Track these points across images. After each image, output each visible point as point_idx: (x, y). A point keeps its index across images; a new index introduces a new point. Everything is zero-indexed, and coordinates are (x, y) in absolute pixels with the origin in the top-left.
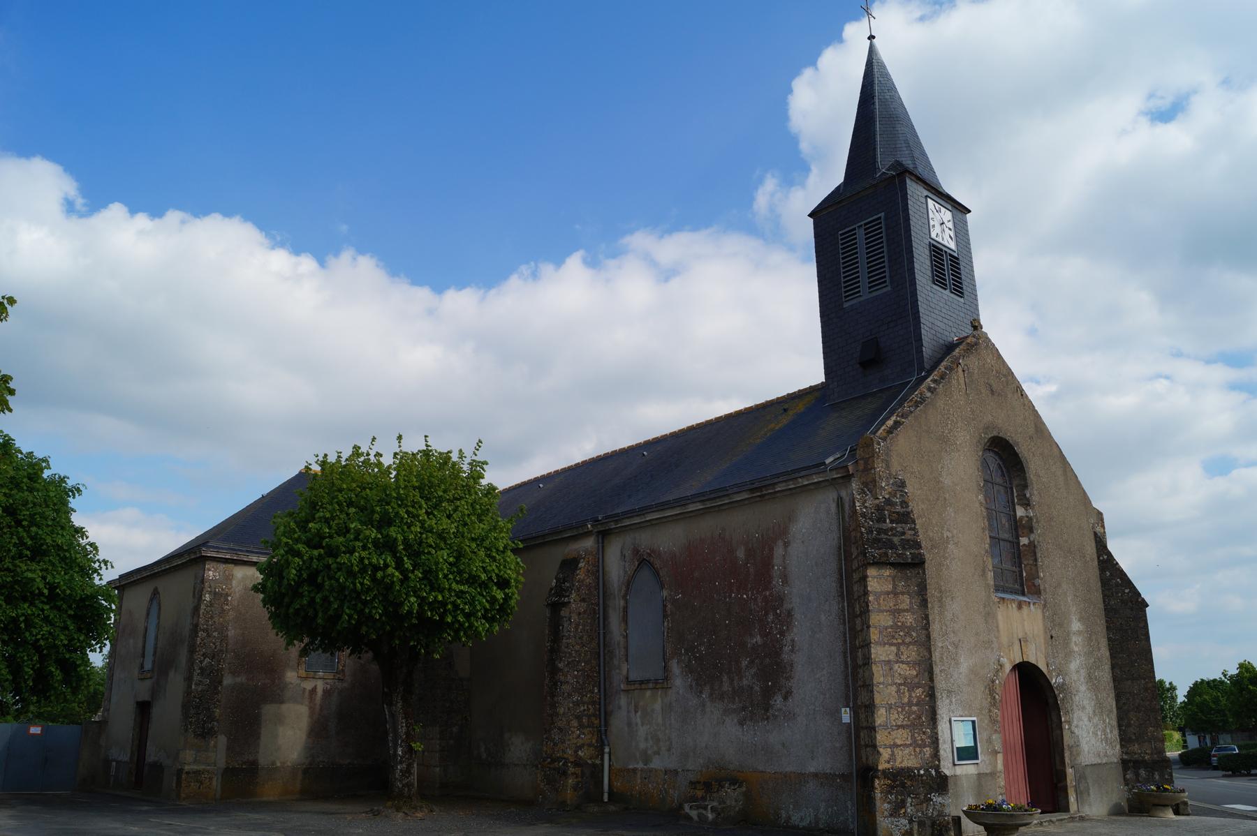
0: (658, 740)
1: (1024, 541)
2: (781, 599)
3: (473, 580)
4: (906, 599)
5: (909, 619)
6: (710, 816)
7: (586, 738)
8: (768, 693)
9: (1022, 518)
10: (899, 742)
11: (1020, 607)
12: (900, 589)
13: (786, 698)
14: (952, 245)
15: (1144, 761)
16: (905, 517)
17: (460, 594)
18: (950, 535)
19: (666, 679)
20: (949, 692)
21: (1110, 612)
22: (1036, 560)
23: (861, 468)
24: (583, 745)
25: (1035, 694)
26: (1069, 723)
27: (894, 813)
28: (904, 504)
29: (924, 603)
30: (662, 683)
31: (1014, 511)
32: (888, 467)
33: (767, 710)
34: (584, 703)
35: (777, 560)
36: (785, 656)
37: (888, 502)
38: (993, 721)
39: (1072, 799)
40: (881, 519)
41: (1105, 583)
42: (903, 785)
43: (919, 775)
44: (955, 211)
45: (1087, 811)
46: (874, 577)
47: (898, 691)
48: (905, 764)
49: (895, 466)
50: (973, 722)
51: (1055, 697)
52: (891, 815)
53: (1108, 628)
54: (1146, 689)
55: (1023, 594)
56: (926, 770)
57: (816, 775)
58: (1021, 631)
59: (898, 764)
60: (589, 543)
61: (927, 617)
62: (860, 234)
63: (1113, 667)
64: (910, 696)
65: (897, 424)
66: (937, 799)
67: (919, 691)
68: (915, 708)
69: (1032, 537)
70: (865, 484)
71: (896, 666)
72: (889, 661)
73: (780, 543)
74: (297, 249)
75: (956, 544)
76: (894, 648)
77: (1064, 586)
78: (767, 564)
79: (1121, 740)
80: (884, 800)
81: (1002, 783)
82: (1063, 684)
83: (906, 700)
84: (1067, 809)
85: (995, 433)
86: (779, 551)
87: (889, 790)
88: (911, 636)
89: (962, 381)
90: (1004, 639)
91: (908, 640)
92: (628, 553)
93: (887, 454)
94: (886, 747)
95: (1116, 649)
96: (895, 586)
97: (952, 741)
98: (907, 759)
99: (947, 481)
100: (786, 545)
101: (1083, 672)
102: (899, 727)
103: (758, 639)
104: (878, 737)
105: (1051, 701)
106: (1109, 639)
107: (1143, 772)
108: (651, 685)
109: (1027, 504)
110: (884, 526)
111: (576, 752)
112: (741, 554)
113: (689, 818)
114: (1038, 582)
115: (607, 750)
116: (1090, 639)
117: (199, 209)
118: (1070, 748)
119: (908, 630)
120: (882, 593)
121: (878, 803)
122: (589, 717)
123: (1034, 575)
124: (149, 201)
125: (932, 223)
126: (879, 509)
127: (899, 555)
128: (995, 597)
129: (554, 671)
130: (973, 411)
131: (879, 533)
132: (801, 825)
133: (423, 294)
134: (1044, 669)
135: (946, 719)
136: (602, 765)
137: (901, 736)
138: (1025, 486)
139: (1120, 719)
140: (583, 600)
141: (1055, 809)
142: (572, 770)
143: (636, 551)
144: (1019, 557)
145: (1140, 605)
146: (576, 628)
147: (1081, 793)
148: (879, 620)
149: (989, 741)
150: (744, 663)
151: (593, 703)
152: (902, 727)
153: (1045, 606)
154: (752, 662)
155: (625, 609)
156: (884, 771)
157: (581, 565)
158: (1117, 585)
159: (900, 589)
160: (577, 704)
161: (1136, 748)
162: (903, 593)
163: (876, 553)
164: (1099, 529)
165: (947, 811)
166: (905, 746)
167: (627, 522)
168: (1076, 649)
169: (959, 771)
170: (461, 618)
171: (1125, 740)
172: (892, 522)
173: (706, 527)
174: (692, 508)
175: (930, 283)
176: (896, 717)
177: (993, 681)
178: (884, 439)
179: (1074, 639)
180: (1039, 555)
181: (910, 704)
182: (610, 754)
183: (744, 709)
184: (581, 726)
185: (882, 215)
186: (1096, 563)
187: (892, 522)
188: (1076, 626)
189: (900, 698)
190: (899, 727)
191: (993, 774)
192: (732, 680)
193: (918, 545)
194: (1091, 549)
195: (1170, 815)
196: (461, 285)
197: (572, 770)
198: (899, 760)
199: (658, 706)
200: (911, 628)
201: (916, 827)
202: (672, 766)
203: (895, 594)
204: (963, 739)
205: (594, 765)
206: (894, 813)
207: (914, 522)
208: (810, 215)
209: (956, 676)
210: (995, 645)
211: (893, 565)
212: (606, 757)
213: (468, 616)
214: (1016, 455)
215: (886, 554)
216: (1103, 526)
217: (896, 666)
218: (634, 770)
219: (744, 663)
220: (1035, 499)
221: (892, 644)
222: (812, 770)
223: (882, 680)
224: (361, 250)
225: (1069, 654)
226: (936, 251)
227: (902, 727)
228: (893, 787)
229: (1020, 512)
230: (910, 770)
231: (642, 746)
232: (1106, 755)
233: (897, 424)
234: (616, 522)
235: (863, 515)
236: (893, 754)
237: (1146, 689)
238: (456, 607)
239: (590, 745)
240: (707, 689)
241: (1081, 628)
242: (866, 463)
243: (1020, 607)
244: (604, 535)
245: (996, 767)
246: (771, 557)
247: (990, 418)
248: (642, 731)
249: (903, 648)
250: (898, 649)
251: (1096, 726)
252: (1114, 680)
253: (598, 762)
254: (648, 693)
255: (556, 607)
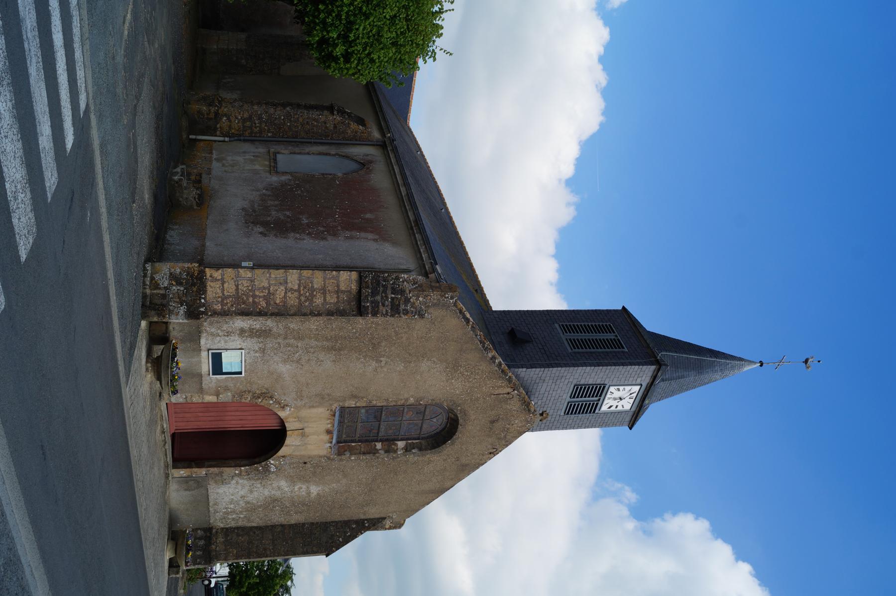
0: (232, 166)
1: (379, 445)
2: (335, 235)
3: (350, 26)
4: (334, 300)
5: (318, 301)
6: (176, 178)
7: (236, 124)
8: (265, 224)
9: (396, 445)
10: (226, 285)
11: (329, 432)
12: (341, 295)
13: (261, 233)
14: (604, 408)
15: (210, 544)
16: (395, 310)
17: (339, 16)
18: (383, 363)
19: (277, 172)
20: (264, 350)
21: (324, 526)
22: (364, 453)
23: (433, 284)
24: (230, 121)
25: (260, 444)
26: (240, 475)
27: (173, 276)
28: (406, 312)
29: (330, 313)
30: (273, 168)
31: (402, 440)
32: (434, 305)
33: (253, 223)
34: (260, 123)
35: (363, 235)
36: (292, 234)
37: (407, 301)
38: (241, 394)
39: (183, 472)
40: (394, 291)
41: (347, 523)
42: (193, 285)
43: (200, 298)
44: (631, 414)
45: (173, 486)
46: (350, 276)
47: (264, 288)
48: (209, 290)
49: (435, 313)
50: (240, 373)
51: (259, 463)
52: (171, 274)
53: (312, 524)
54: (265, 549)
55: (338, 442)
56: (204, 305)
57: (204, 245)
58: (310, 433)
59: (209, 283)
60: (376, 135)
61: (319, 315)
62: (611, 336)
63: (282, 526)
64: (260, 297)
65: (467, 321)
66: (182, 310)
67: (263, 304)
68: (251, 300)
69: (382, 452)
70: (421, 286)
71: (283, 288)
72: (286, 283)
73: (377, 237)
74: (580, 163)
75: (376, 370)
76: (296, 287)
77: (344, 481)
78: (361, 229)
79: (227, 529)
80: (182, 269)
81: (194, 400)
82: (270, 471)
83: (257, 293)
84: (174, 467)
85: (461, 421)
86: (370, 236)
87: (189, 273)
88: (306, 301)
89: (501, 391)
90: (305, 413)
91: (303, 299)
92: (369, 158)
93: (444, 305)
94: (222, 275)
95: (297, 528)
96: (343, 292)
97: (227, 349)
98: (213, 291)
99: (425, 365)
100: (375, 240)
101: (278, 494)
102: (237, 286)
103: (305, 221)
104: (230, 270)
105: (257, 460)
106: (304, 524)
107: (202, 543)
108: (272, 164)
109: (407, 449)
110: (389, 291)
111: (225, 115)
112: (368, 216)
113: (175, 167)
114: (348, 454)
115: (227, 139)
116: (304, 504)
117: (606, 93)
118: (221, 473)
119: (310, 299)
120: (338, 281)
121: (180, 265)
122: (251, 128)
123: (352, 451)
124: (609, 59)
125: (621, 388)
126: (402, 292)
127: (367, 296)
128: (336, 406)
129: (284, 105)
130: (477, 399)
131: (383, 286)
132: (168, 237)
133: (552, 250)
134: (280, 453)
135: (244, 345)
136: (216, 136)
137: (230, 288)
138: (420, 449)
139: (243, 529)
140: (335, 127)
141: (175, 460)
142: (213, 109)
143: (371, 162)
144: (366, 441)
145: (328, 549)
146: (314, 120)
147: (187, 482)
148: (318, 279)
149: (227, 389)
150: (288, 213)
151: (261, 132)
152: (237, 289)
153: (329, 458)
154: (288, 217)
155: (329, 154)
156: (204, 272)
157: (361, 127)
158: (345, 533)
159: (341, 295)
160: (260, 118)
161: (221, 539)
162: (338, 297)
163: (369, 279)
164: (388, 523)
165: (173, 317)
166: (223, 290)
167: (392, 156)
168: (296, 488)
169: (204, 354)
170: (322, 16)
171: (227, 531)
172: (392, 299)
173: (390, 199)
174: (403, 189)
175: (575, 382)
176: (244, 285)
177: (271, 398)
178: (455, 304)
179: (304, 487)
180: (368, 456)
181: (254, 296)
182: (224, 141)
183: (254, 211)
184: (244, 120)
185: (626, 350)
186: (362, 517)
187: (392, 299)
188: (315, 490)
189: (259, 289)
190: (237, 286)
191: (201, 390)
192: (276, 206)
193: (375, 314)
194: (373, 512)
195: (168, 555)
196: (560, 271)
197: (213, 109)
198: (212, 284)
199: (257, 167)
200: (311, 301)
201: (162, 292)
202: (214, 172)
203: (338, 292)
204: (231, 360)
205: (215, 129)
206: (173, 276)
207: (392, 316)
208: (624, 307)
209: (276, 358)
210: (299, 403)
211: (359, 292)
212: (221, 139)
213: (324, 22)
214: (444, 442)
215: (368, 287)
216: (390, 528)
217: (283, 288)
218: (211, 153)
219: (288, 213)
220: (411, 458)
221: (299, 286)
222: (208, 244)
223: (273, 276)
224: (579, 207)
225: (292, 480)
226: (600, 391)
227: (237, 289)
228: (192, 276)
229: (401, 444)
230: (205, 292)
231: (229, 158)
232: (216, 512)
233: (467, 321)
234: (392, 150)
235: (397, 278)
236: (217, 280)
237: (265, 549)
238: (329, 13)
239: (230, 127)
240: (269, 193)
241: (313, 496)
242: (436, 287)
243: (329, 432)
244: (383, 146)
245: (207, 394)
246: (366, 231)
247: (473, 417)
248: (240, 159)
249: (296, 294)
250: (295, 291)
251: (237, 503)
252: (272, 526)
253: (218, 133)
254: (267, 163)
255: (331, 109)
